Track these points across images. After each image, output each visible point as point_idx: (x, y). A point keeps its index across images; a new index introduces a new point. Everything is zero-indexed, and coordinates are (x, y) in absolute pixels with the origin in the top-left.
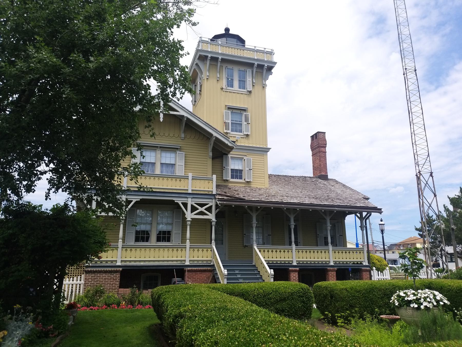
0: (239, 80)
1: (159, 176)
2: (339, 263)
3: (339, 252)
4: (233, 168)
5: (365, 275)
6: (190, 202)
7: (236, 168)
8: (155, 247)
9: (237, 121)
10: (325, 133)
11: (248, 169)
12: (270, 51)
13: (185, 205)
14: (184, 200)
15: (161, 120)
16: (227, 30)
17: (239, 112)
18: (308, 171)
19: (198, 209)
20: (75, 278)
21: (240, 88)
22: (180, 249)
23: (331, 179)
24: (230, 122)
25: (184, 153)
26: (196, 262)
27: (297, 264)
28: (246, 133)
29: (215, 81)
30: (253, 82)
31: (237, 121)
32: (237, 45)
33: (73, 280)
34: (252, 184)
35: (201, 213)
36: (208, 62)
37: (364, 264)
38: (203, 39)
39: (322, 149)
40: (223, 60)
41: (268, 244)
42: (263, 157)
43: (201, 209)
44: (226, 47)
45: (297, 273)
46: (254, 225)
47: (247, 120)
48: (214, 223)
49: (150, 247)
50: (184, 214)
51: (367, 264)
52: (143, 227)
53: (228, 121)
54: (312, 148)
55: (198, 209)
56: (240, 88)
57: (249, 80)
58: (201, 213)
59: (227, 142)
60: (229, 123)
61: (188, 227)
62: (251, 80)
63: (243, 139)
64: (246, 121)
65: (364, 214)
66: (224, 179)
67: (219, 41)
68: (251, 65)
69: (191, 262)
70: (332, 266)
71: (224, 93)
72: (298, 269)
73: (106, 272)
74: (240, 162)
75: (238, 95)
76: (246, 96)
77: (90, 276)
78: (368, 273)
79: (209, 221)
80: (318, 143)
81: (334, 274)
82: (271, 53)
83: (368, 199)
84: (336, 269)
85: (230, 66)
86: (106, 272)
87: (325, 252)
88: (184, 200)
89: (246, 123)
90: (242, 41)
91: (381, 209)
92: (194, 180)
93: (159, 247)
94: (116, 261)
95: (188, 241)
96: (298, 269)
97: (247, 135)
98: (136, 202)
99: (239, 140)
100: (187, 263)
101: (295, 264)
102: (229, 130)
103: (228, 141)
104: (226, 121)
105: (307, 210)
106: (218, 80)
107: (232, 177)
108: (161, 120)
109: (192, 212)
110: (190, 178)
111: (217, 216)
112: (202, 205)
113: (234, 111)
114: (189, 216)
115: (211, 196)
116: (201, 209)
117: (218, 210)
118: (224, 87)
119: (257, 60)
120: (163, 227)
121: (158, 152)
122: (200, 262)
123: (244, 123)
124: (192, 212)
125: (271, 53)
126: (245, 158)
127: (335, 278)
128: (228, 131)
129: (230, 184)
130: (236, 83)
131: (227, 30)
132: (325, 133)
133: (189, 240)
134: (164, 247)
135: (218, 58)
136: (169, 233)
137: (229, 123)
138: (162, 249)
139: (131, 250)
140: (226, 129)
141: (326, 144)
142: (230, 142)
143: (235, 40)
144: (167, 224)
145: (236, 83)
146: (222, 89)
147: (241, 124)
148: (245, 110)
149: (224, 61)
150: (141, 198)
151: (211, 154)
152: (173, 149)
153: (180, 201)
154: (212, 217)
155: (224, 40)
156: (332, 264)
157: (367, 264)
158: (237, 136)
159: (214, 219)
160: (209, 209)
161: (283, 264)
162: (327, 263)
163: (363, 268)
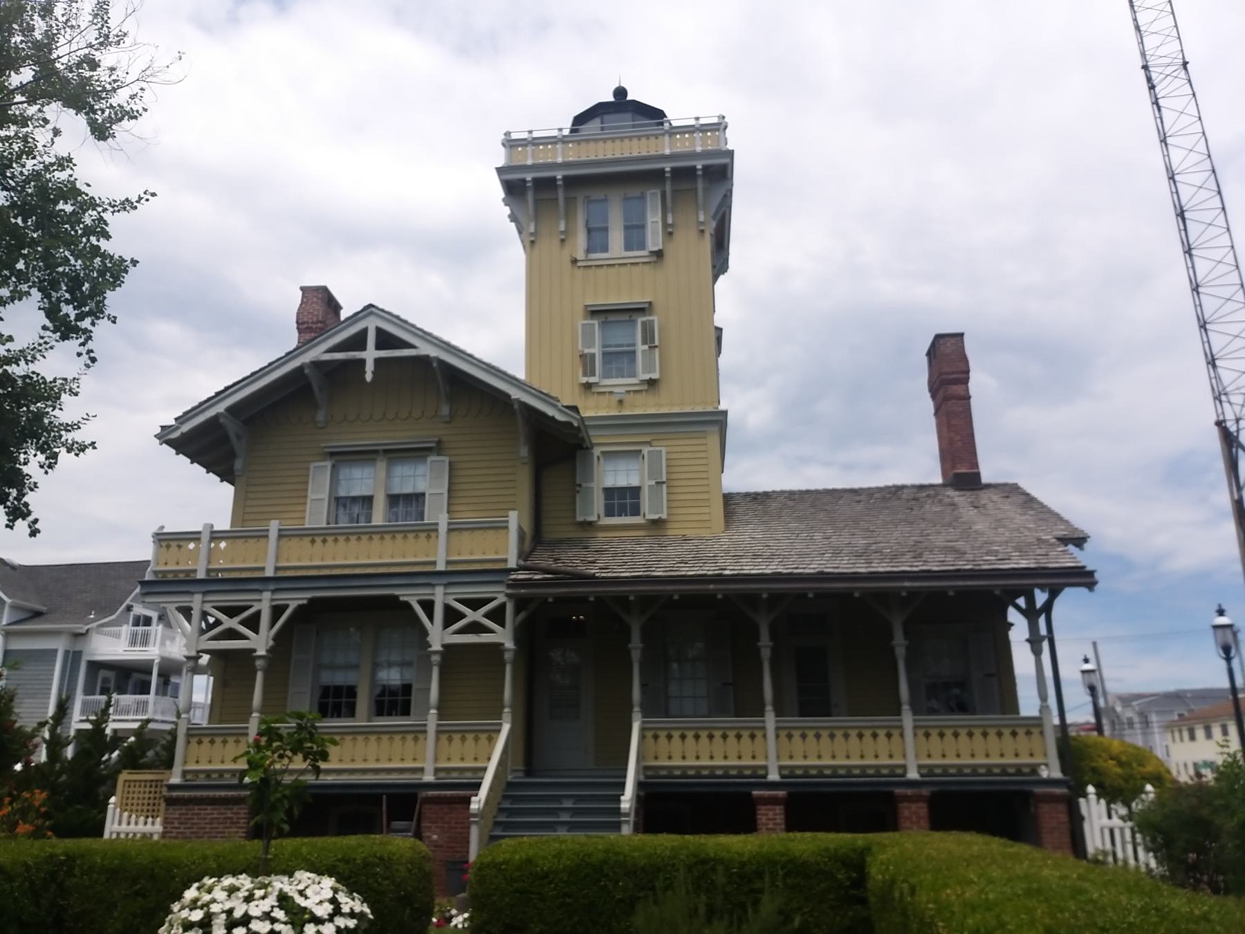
0: (626, 228)
1: (381, 532)
2: (945, 774)
3: (970, 735)
4: (610, 482)
5: (1052, 818)
6: (440, 596)
7: (622, 482)
8: (366, 732)
9: (622, 346)
10: (962, 335)
11: (653, 483)
12: (715, 120)
13: (428, 606)
14: (424, 593)
15: (369, 377)
16: (620, 92)
17: (625, 317)
18: (919, 463)
19: (463, 616)
20: (134, 816)
21: (628, 247)
22: (219, 740)
23: (989, 486)
24: (596, 350)
25: (446, 459)
26: (455, 774)
27: (782, 777)
28: (647, 377)
29: (556, 243)
30: (665, 225)
31: (622, 346)
32: (634, 126)
33: (146, 823)
34: (669, 525)
35: (475, 628)
36: (530, 197)
37: (1044, 774)
38: (514, 136)
39: (957, 389)
40: (571, 182)
41: (723, 713)
42: (703, 441)
43: (472, 616)
44: (605, 140)
45: (779, 809)
46: (636, 655)
47: (648, 336)
48: (508, 656)
49: (355, 732)
50: (425, 633)
51: (1057, 774)
52: (340, 679)
53: (591, 351)
54: (934, 390)
55: (463, 616)
56: (628, 247)
57: (654, 220)
58: (475, 628)
59: (550, 412)
60: (593, 356)
61: (260, 676)
62: (659, 218)
63: (638, 396)
64: (644, 342)
65: (1041, 598)
66: (580, 519)
67: (593, 126)
68: (652, 177)
69: (442, 775)
70: (773, 785)
71: (579, 273)
72: (781, 793)
73: (213, 802)
74: (634, 465)
75: (623, 269)
76: (647, 268)
77: (176, 812)
78: (1062, 807)
79: (497, 648)
80: (948, 366)
81: (922, 809)
82: (719, 127)
83: (1079, 541)
84: (925, 792)
85: (597, 194)
86: (213, 802)
87: (889, 736)
88: (424, 593)
89: (646, 347)
90: (656, 115)
91: (1091, 574)
92: (454, 534)
93: (379, 732)
94: (422, 770)
95: (506, 710)
96: (781, 793)
97: (652, 383)
98: (300, 608)
99: (627, 398)
100: (429, 778)
101: (774, 776)
102: (593, 374)
103: (555, 406)
104: (586, 351)
105: (940, 594)
106: (532, 242)
107: (609, 512)
108: (369, 377)
109: (446, 625)
110: (273, 534)
111: (521, 635)
112: (474, 604)
113: (611, 318)
114: (438, 636)
115: (497, 573)
116: (472, 616)
117: (522, 615)
118: (580, 255)
119: (672, 157)
120: (392, 677)
121: (381, 465)
122: (469, 774)
123: (641, 348)
124: (446, 625)
125: (719, 127)
126: (646, 450)
127: (925, 823)
128: (592, 380)
129: (601, 535)
130: (616, 238)
131: (620, 92)
132: (962, 335)
133: (261, 712)
134: (391, 732)
135: (662, 171)
136: (407, 689)
137: (593, 356)
138: (360, 738)
139: (212, 742)
140: (585, 375)
141: (968, 372)
142: (560, 410)
143: (629, 116)
144: (403, 664)
145: (616, 238)
146: (574, 261)
147: (634, 352)
148: (641, 310)
149: (573, 183)
150: (309, 595)
151: (524, 451)
152: (415, 453)
153: (411, 596)
154: (503, 636)
155: (613, 120)
156: (913, 775)
157: (1057, 774)
158: (616, 390)
159: (509, 644)
160: (497, 615)
161: (966, 775)
162: (758, 774)
163: (1038, 790)
